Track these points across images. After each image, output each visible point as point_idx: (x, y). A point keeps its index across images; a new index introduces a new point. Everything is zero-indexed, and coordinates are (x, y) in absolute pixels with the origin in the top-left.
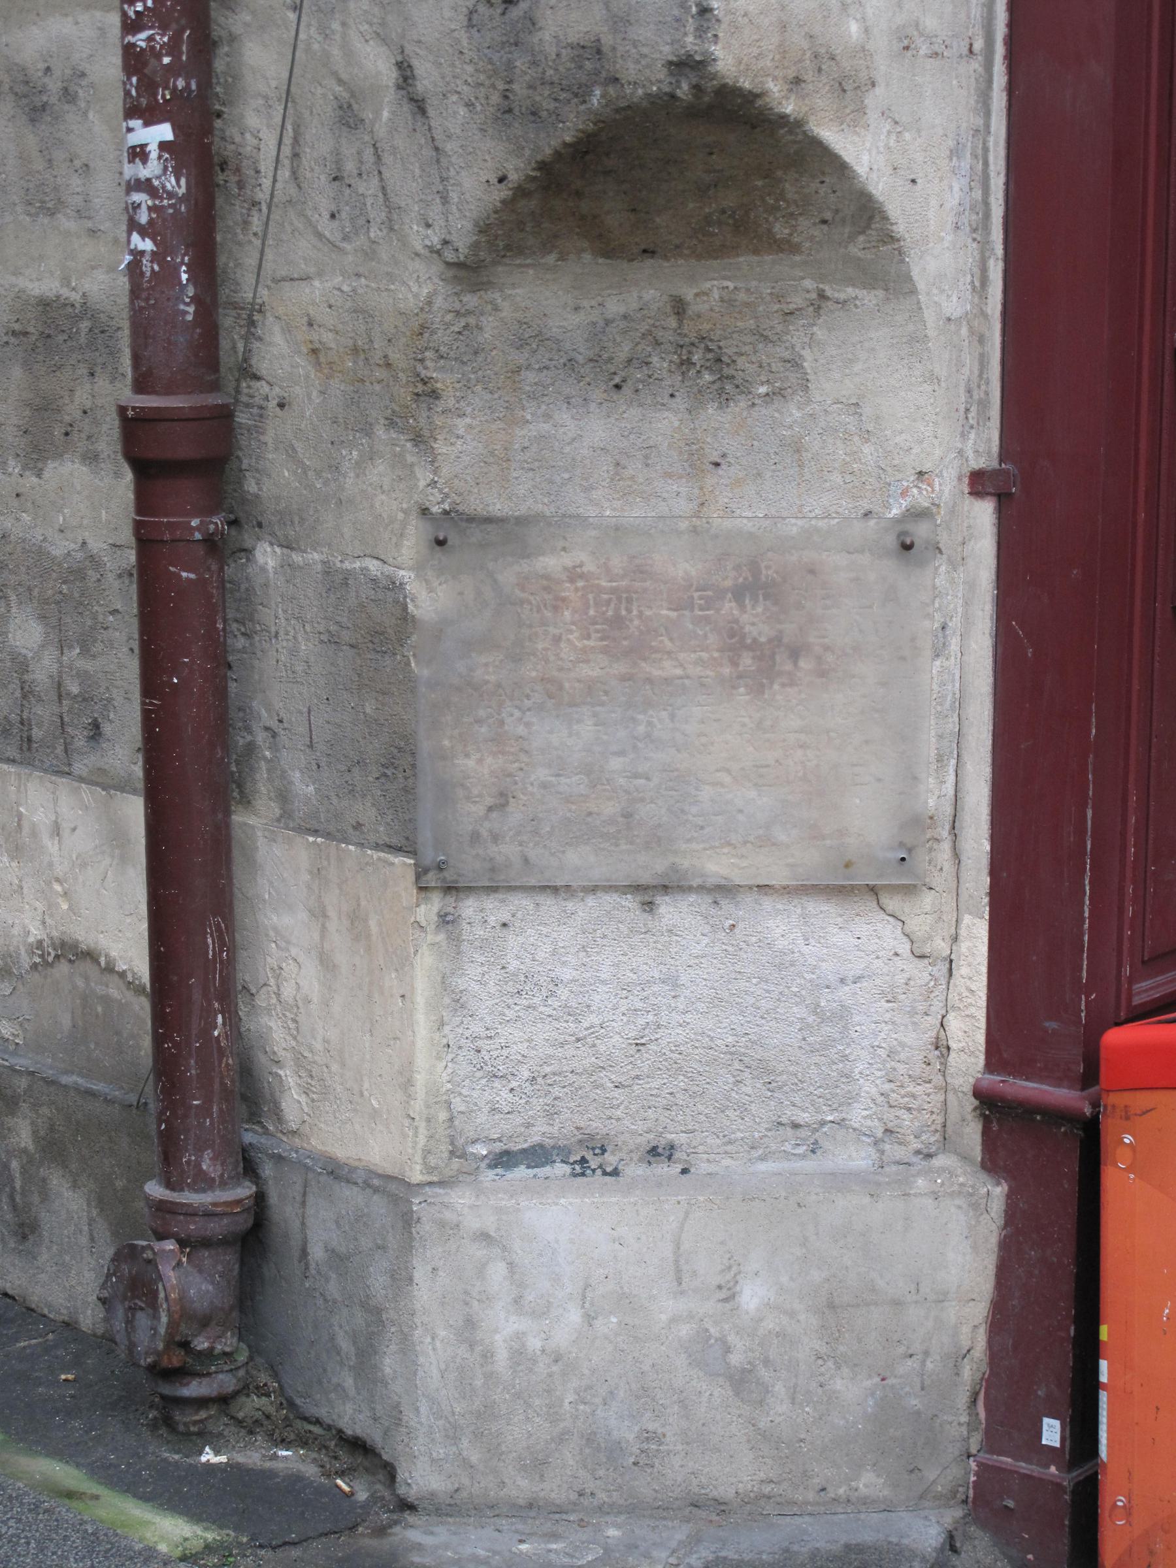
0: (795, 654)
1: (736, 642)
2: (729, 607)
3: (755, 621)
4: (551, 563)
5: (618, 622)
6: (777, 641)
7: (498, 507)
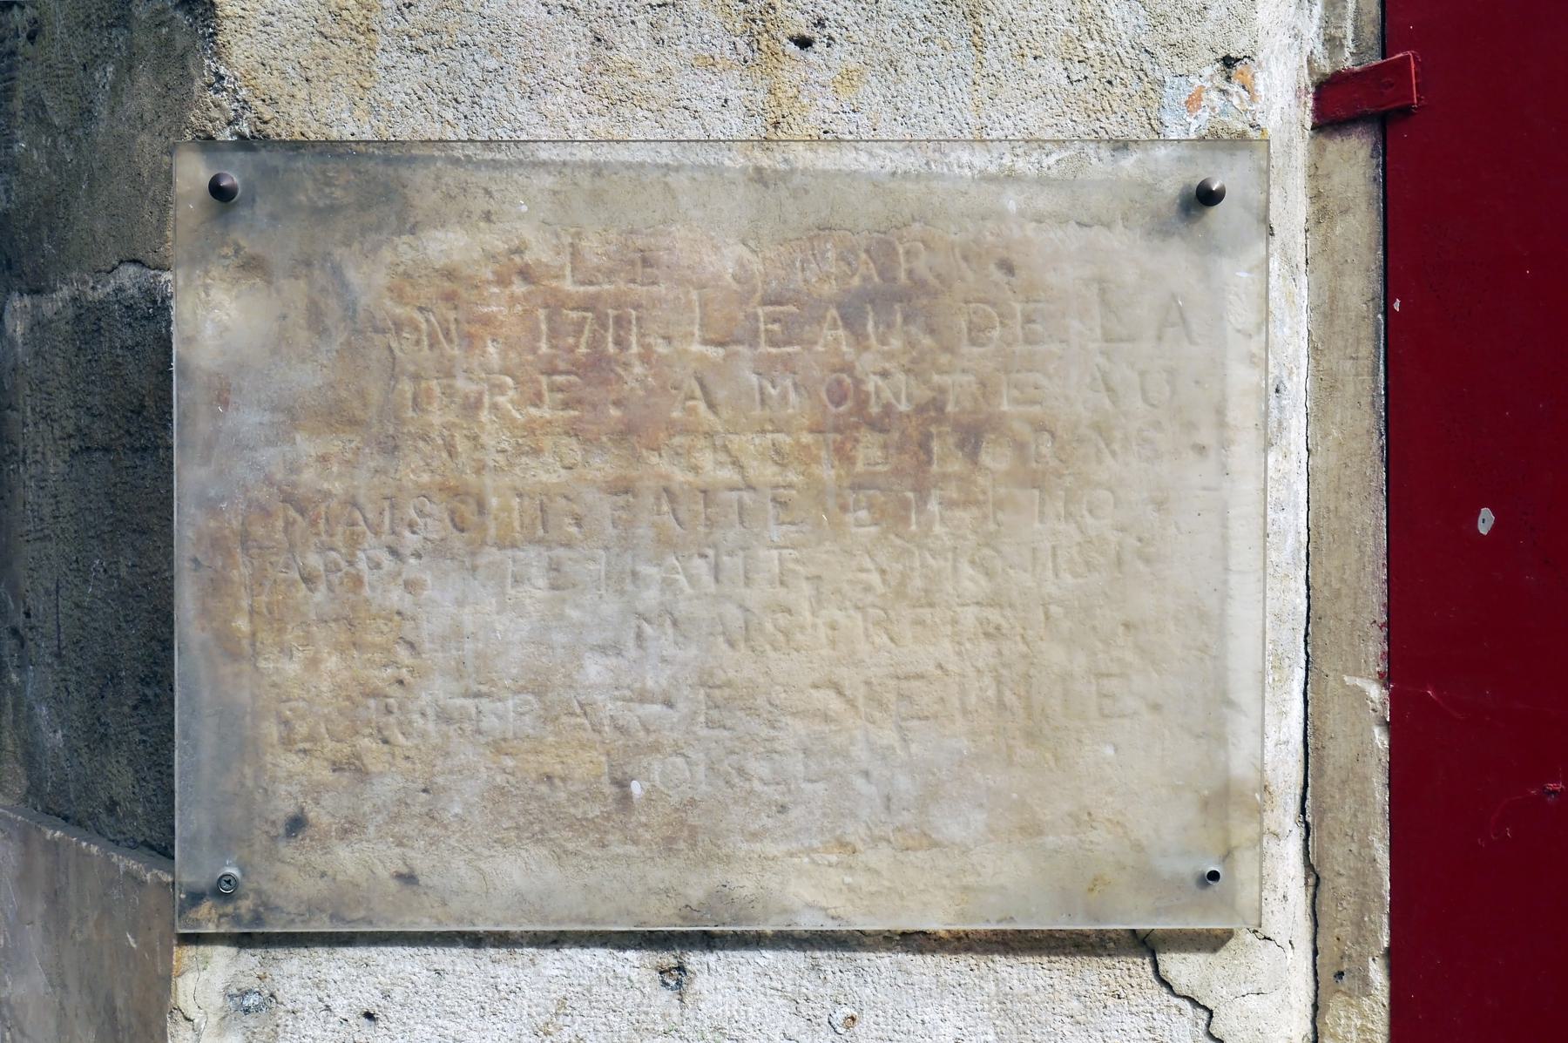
0: (971, 437)
1: (849, 413)
2: (832, 338)
3: (883, 368)
4: (448, 244)
5: (597, 367)
6: (932, 409)
7: (351, 126)
